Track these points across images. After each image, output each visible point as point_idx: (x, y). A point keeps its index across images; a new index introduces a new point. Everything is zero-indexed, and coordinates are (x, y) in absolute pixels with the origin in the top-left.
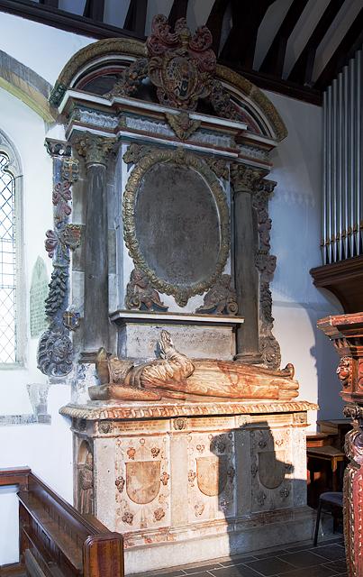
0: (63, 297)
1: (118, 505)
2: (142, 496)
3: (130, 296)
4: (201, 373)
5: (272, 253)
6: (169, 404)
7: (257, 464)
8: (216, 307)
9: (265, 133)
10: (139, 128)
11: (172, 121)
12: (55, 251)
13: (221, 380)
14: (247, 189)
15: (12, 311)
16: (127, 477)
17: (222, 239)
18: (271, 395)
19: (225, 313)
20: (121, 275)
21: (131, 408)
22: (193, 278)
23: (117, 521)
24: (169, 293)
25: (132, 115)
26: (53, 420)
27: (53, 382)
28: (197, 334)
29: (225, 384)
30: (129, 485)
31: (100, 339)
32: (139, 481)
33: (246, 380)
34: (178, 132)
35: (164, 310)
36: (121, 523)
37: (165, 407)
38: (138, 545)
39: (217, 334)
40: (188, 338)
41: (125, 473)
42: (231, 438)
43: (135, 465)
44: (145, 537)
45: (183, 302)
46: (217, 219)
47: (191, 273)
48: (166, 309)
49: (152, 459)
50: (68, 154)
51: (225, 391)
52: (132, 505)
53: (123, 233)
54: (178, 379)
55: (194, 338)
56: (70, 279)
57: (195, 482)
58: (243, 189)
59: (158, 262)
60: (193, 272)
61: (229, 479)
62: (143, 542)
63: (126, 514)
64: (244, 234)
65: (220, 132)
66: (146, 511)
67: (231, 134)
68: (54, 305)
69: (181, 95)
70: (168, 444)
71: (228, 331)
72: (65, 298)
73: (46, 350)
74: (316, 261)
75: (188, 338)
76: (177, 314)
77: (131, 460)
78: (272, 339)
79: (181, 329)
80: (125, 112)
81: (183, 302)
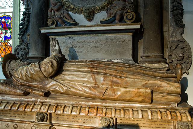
10: (58, 34)
18: (140, 99)
19: (121, 20)
24: (80, 12)
31: (34, 48)
35: (76, 24)
40: (93, 44)
45: (90, 16)
55: (98, 44)
75: (93, 44)
76: (88, 26)
78: (183, 41)
79: (88, 37)
81: (90, 16)
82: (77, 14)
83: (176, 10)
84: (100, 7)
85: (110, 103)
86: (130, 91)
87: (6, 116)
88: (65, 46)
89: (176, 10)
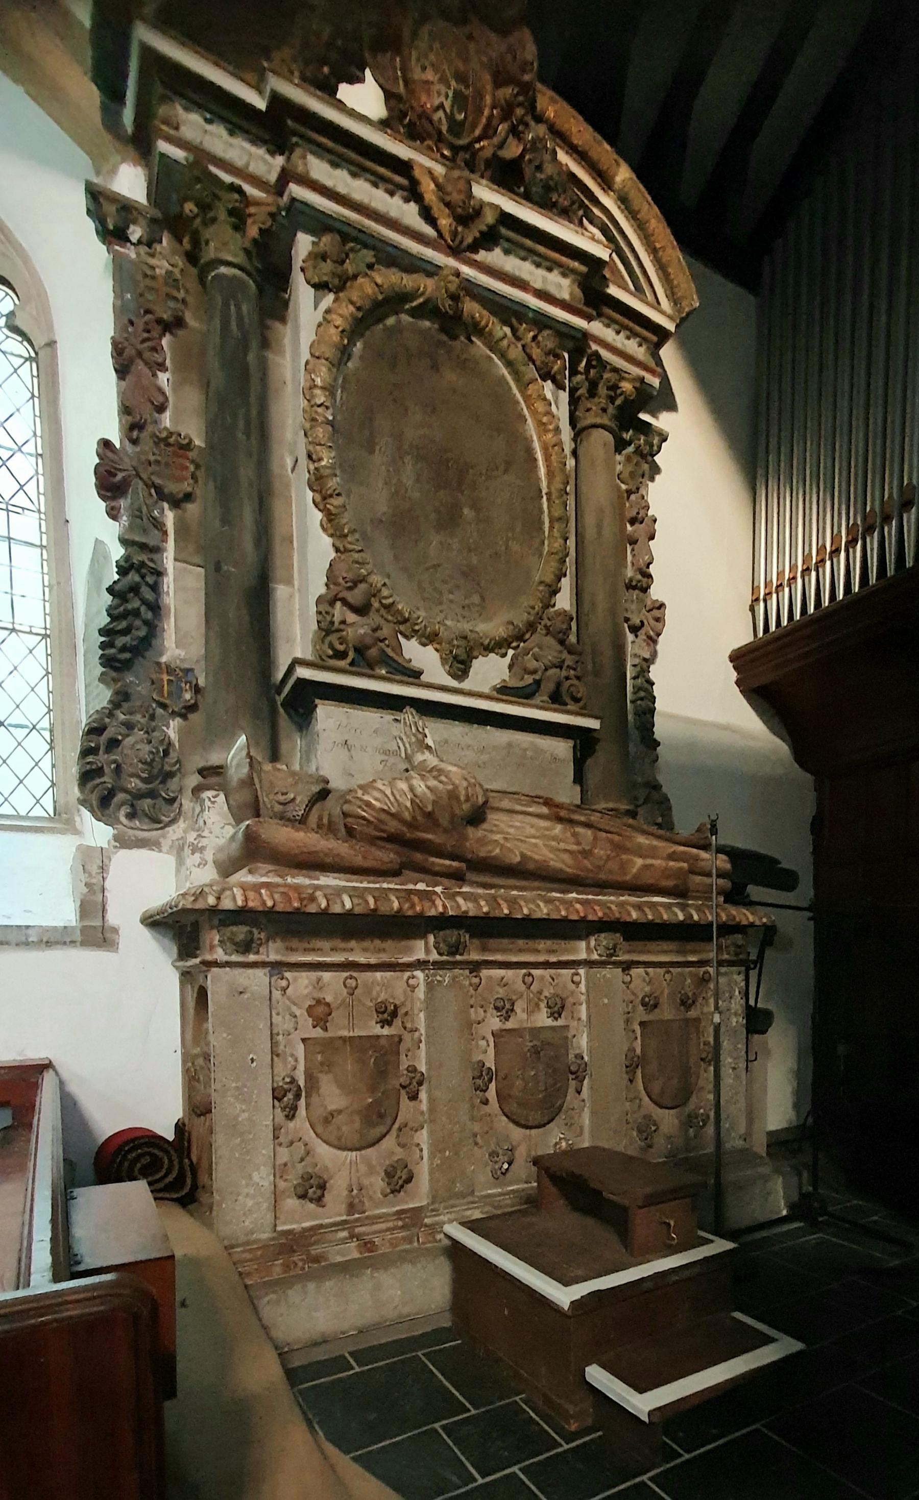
0: (146, 623)
1: (284, 1155)
2: (349, 1128)
3: (327, 629)
4: (504, 817)
5: (656, 592)
6: (421, 886)
7: (638, 1051)
8: (538, 683)
9: (638, 288)
11: (428, 188)
12: (123, 503)
13: (554, 838)
14: (605, 420)
15: (42, 690)
16: (309, 1076)
17: (551, 528)
19: (557, 700)
20: (303, 591)
21: (318, 888)
22: (483, 611)
23: (277, 1197)
24: (429, 638)
25: (322, 151)
26: (123, 940)
27: (122, 842)
28: (495, 748)
29: (562, 845)
30: (315, 1099)
32: (341, 1085)
33: (611, 842)
34: (445, 222)
35: (414, 675)
36: (291, 1203)
37: (410, 892)
38: (339, 1259)
39: (539, 751)
41: (301, 1067)
42: (577, 984)
43: (329, 1045)
44: (358, 1237)
46: (539, 479)
47: (476, 599)
48: (417, 674)
49: (377, 1030)
50: (149, 242)
51: (561, 862)
52: (323, 1151)
53: (301, 477)
54: (444, 821)
55: (485, 757)
56: (169, 583)
57: (492, 1093)
58: (598, 421)
59: (396, 557)
60: (483, 598)
61: (573, 1084)
62: (352, 1251)
63: (307, 1177)
64: (599, 526)
65: (546, 258)
66: (363, 1168)
67: (573, 271)
68: (121, 641)
69: (450, 130)
70: (421, 993)
71: (562, 748)
72: (153, 630)
73: (102, 758)
74: (743, 637)
77: (318, 1033)
79: (457, 731)
80: (301, 136)
82: (413, 640)
83: (642, 699)
84: (491, 640)
85: (611, 895)
86: (652, 865)
87: (314, 950)
88: (380, 746)
89: (642, 699)
